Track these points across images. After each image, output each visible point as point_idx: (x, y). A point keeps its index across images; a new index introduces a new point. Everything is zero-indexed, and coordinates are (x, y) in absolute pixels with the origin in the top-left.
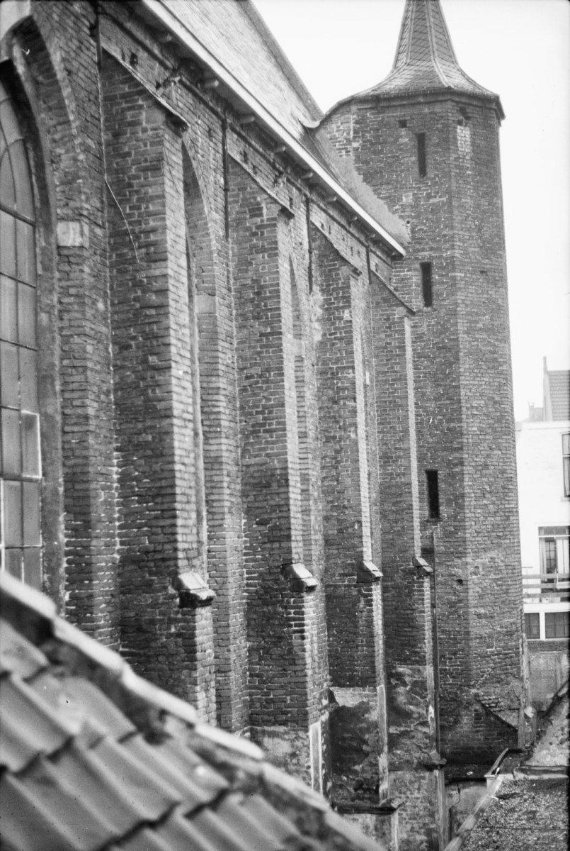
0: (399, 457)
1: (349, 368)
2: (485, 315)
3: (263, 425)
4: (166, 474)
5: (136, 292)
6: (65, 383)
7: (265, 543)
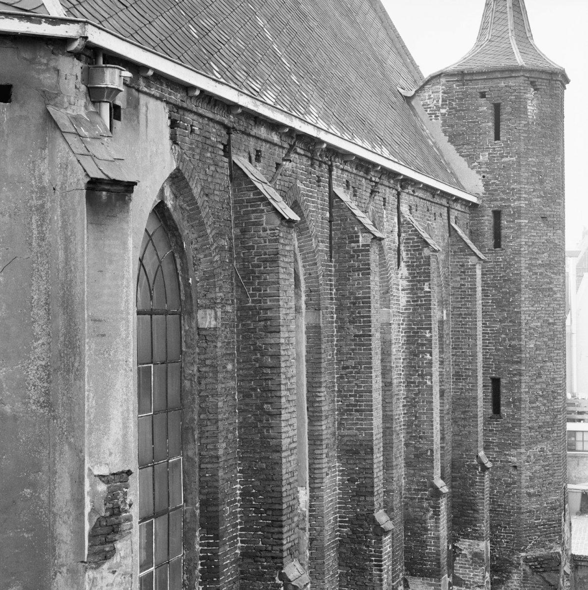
0: (469, 376)
1: (427, 329)
2: (543, 253)
3: (355, 405)
4: (275, 494)
5: (256, 355)
6: (202, 432)
7: (354, 496)
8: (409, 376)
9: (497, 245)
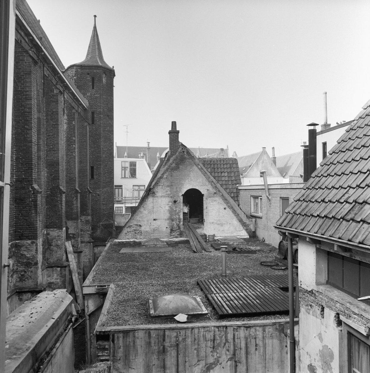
8: (67, 153)
9: (93, 123)
